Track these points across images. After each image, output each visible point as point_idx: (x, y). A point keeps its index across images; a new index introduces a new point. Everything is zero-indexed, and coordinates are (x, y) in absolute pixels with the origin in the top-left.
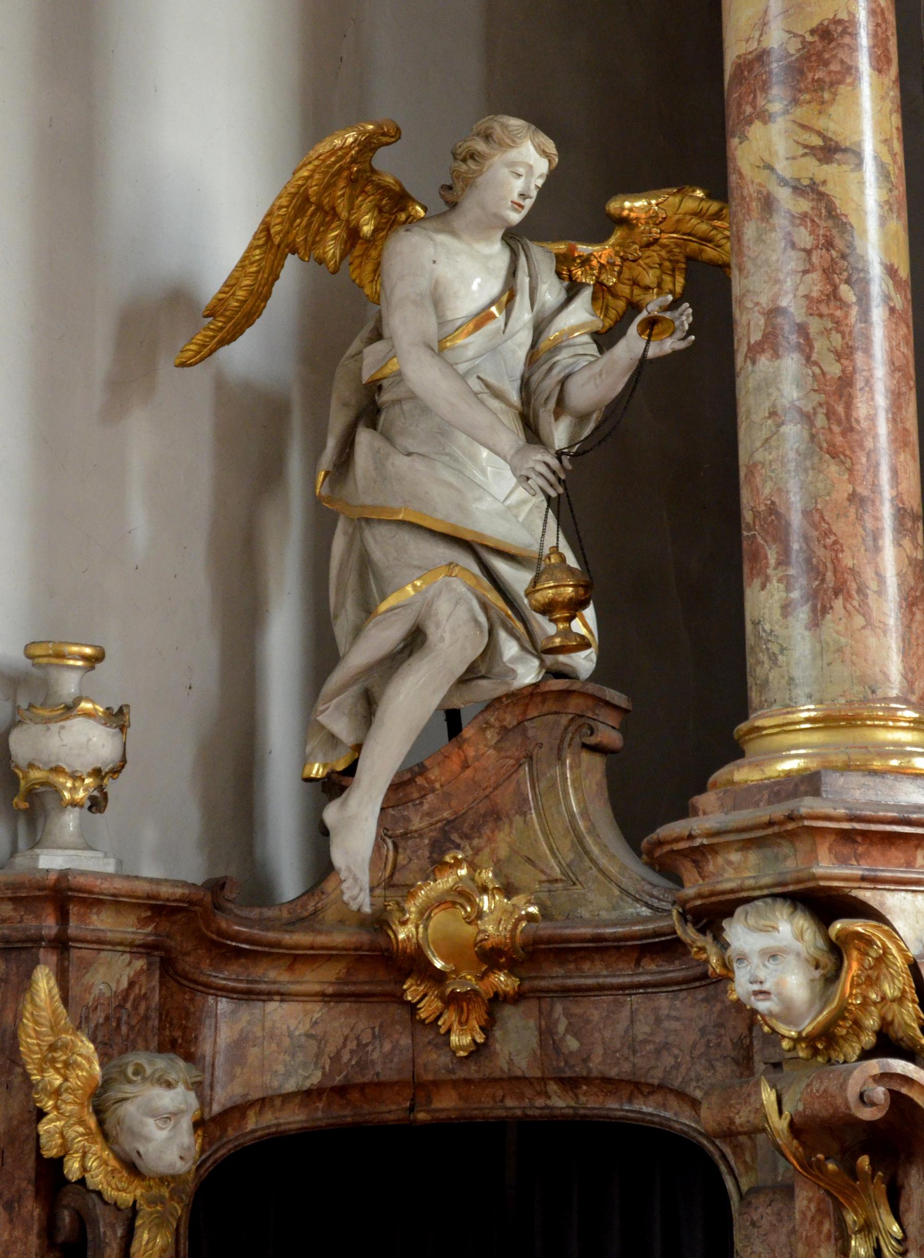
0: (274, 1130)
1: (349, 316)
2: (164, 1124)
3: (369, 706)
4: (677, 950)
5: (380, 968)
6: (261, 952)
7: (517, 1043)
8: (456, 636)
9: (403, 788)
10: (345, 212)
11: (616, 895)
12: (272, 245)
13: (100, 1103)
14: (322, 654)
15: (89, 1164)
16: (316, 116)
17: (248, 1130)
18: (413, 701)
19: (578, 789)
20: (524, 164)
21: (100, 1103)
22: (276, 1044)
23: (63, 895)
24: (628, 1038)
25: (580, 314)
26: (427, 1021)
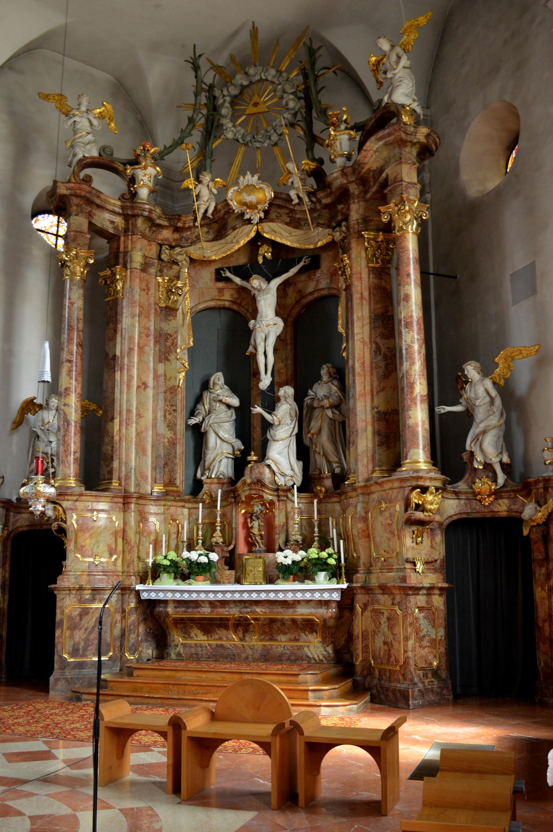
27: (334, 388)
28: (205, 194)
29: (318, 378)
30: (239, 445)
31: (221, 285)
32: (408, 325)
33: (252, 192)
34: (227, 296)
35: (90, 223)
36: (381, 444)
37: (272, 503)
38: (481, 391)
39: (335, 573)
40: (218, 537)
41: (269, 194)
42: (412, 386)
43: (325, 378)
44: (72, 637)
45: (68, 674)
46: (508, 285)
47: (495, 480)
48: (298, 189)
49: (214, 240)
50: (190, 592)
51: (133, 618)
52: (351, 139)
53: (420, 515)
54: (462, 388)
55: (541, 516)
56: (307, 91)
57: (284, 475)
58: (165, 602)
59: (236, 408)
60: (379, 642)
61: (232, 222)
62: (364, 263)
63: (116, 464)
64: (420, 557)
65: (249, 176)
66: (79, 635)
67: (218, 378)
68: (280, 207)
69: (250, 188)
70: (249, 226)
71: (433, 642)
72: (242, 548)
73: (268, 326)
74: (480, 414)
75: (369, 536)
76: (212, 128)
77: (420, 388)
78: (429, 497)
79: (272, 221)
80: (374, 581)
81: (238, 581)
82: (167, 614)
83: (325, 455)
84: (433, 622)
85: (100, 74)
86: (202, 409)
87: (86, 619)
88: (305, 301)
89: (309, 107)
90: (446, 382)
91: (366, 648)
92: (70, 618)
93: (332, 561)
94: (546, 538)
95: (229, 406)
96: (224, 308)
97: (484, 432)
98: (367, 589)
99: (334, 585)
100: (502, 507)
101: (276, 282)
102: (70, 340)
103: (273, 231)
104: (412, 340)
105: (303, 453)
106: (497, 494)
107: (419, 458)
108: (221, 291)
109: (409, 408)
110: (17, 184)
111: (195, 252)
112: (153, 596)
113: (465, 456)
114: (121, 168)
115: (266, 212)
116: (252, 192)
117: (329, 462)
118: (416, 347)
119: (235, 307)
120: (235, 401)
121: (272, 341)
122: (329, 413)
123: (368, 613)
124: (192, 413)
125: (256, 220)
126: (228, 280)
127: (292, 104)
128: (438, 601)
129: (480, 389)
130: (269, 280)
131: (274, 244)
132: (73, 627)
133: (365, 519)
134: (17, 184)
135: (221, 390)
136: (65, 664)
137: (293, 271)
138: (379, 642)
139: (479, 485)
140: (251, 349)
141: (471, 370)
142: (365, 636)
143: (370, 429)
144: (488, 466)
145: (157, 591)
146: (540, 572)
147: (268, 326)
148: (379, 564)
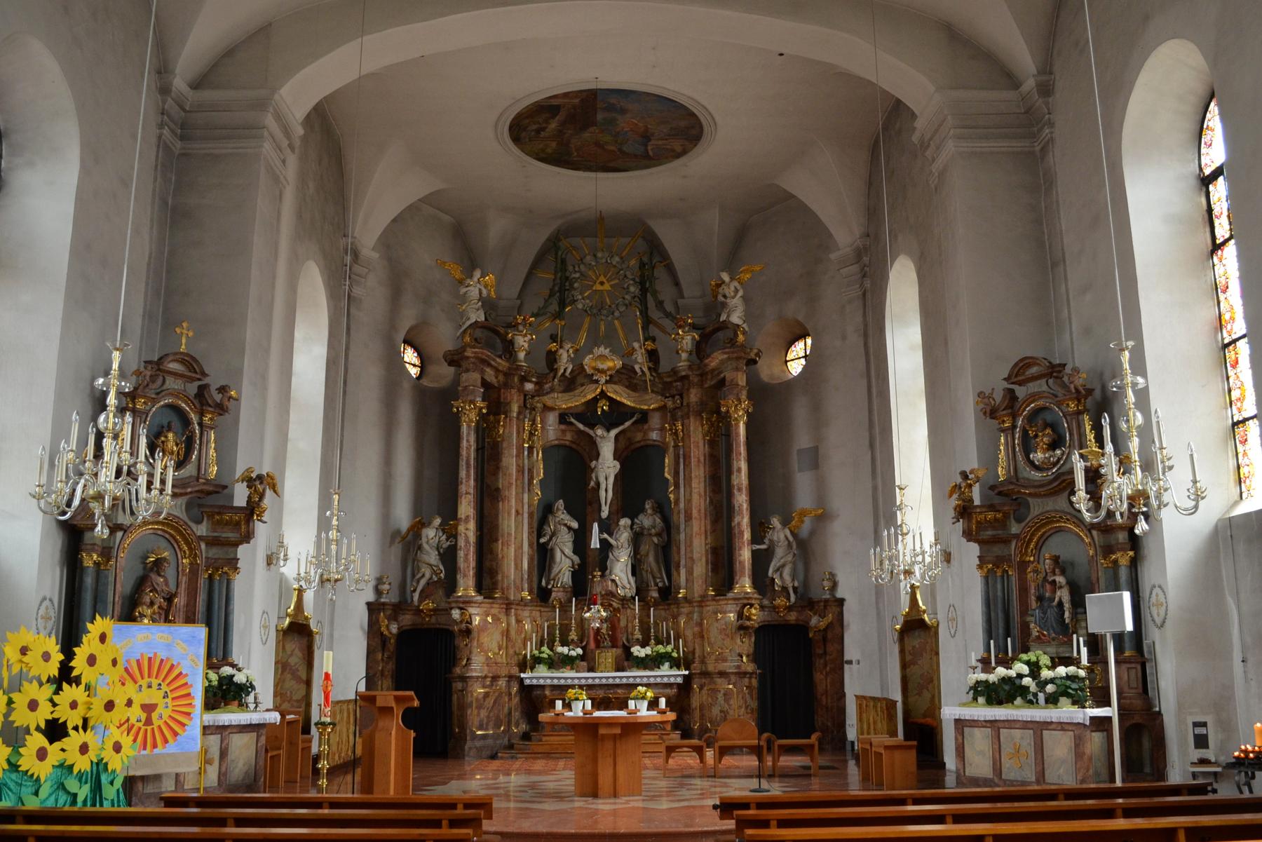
0: (802, 440)
1: (418, 536)
2: (394, 628)
3: (418, 582)
4: (448, 611)
5: (418, 611)
6: (457, 454)
7: (433, 620)
8: (428, 575)
9: (422, 591)
10: (418, 527)
11: (443, 605)
12: (409, 531)
13: (387, 627)
14: (413, 576)
15: (386, 633)
16: (415, 517)
17: (1212, 104)
18: (423, 582)
19: (441, 592)
20: (438, 521)
21: (387, 627)
22: (407, 619)
23: (384, 604)
24: (442, 619)
25: (444, 537)
26: (575, 525)
27: (658, 520)
28: (565, 356)
29: (643, 510)
30: (576, 559)
31: (563, 427)
32: (740, 490)
33: (604, 360)
34: (569, 437)
35: (483, 379)
36: (713, 570)
37: (618, 610)
38: (782, 536)
39: (676, 664)
40: (573, 636)
41: (619, 364)
42: (742, 533)
43: (649, 511)
44: (478, 714)
45: (478, 744)
46: (795, 457)
47: (789, 599)
48: (640, 361)
49: (564, 391)
50: (559, 678)
51: (516, 700)
52: (693, 338)
53: (748, 623)
54: (765, 532)
55: (823, 624)
56: (642, 276)
57: (624, 587)
58: (543, 687)
59: (575, 531)
60: (716, 711)
61: (580, 380)
62: (700, 436)
63: (500, 577)
64: (735, 654)
65: (602, 349)
66: (483, 713)
67: (560, 504)
68: (626, 376)
69: (602, 357)
70: (594, 386)
71: (752, 710)
72: (592, 645)
73: (607, 467)
74: (780, 552)
75: (703, 637)
76: (562, 293)
77: (747, 535)
78: (753, 611)
79: (615, 383)
80: (711, 668)
81: (591, 669)
82: (545, 696)
83: (652, 573)
84: (751, 694)
85: (446, 218)
86: (548, 531)
87: (488, 700)
88: (633, 447)
89: (644, 291)
90: (760, 529)
91: (702, 716)
92: (477, 699)
93: (675, 655)
94: (825, 639)
95: (570, 528)
96: (565, 446)
97: (783, 566)
98: (705, 674)
99: (675, 672)
100: (792, 617)
101: (614, 432)
102: (468, 476)
103: (615, 392)
104: (742, 500)
105: (635, 571)
106: (790, 609)
107: (745, 585)
108: (563, 432)
109: (740, 549)
110: (392, 326)
111: (548, 400)
112: (535, 682)
113: (768, 582)
114: (502, 331)
115: (611, 376)
116: (604, 360)
117: (654, 578)
118: (745, 506)
119: (574, 446)
120: (575, 525)
121: (611, 480)
122: (655, 540)
123: (704, 691)
124: (539, 535)
125: (603, 380)
126: (571, 424)
127: (632, 289)
128: (755, 682)
129: (779, 534)
130: (608, 431)
131: (611, 400)
132: (479, 707)
133: (700, 624)
134: (392, 326)
135: (563, 518)
136: (475, 737)
137: (627, 424)
138: (716, 711)
139: (778, 602)
140: (592, 484)
141: (775, 522)
142: (702, 707)
143: (704, 559)
144: (785, 589)
145: (538, 678)
146: (819, 663)
147: (607, 467)
148: (713, 657)
